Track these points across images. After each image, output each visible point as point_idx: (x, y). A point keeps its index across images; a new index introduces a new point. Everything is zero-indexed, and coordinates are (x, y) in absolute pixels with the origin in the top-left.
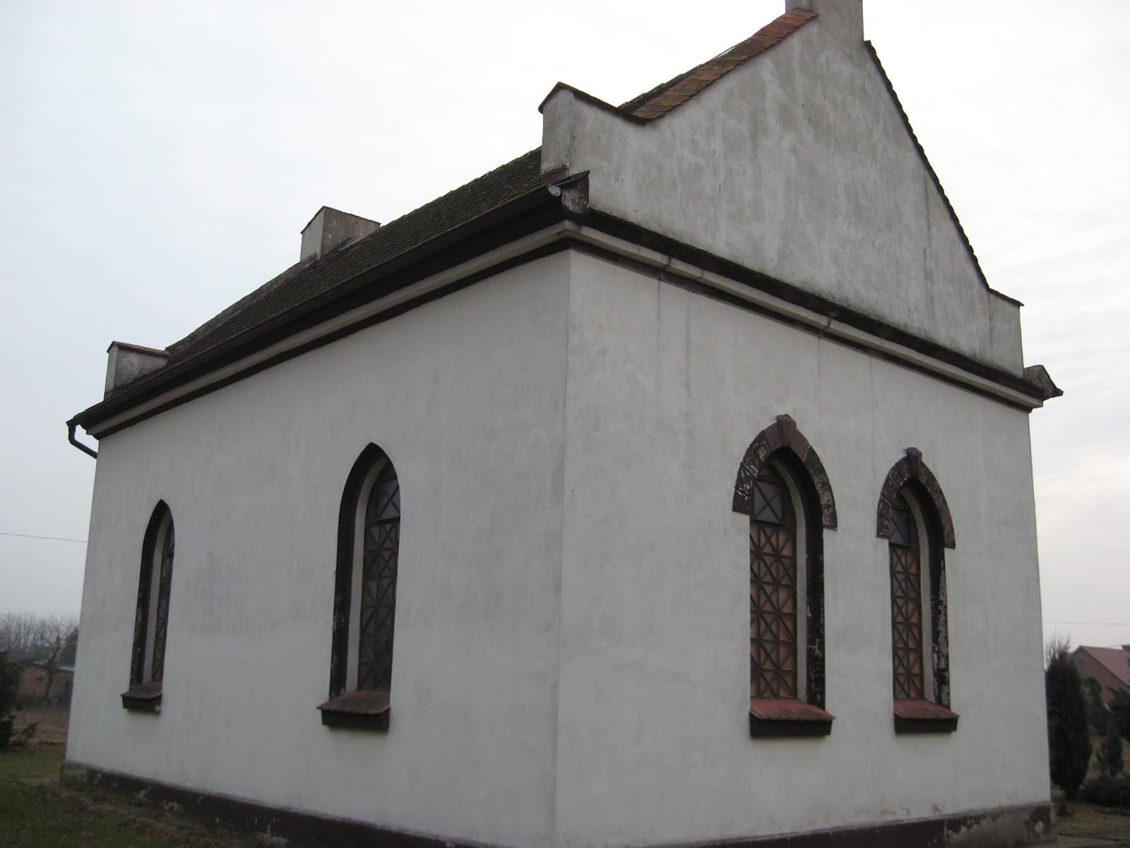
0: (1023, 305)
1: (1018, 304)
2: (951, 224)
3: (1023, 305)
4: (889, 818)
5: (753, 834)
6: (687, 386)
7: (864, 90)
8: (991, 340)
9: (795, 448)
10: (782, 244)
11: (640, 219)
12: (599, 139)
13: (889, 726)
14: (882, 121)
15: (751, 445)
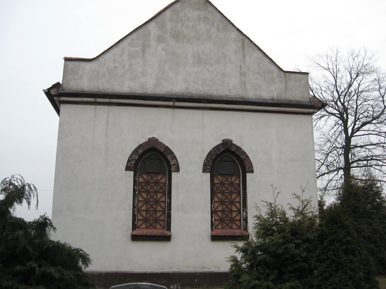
0: (309, 73)
1: (307, 74)
2: (259, 53)
3: (309, 73)
4: (206, 270)
5: (132, 271)
6: (106, 135)
7: (206, 18)
8: (286, 91)
9: (158, 147)
10: (156, 82)
11: (89, 89)
12: (74, 70)
13: (208, 239)
14: (216, 25)
15: (135, 149)
